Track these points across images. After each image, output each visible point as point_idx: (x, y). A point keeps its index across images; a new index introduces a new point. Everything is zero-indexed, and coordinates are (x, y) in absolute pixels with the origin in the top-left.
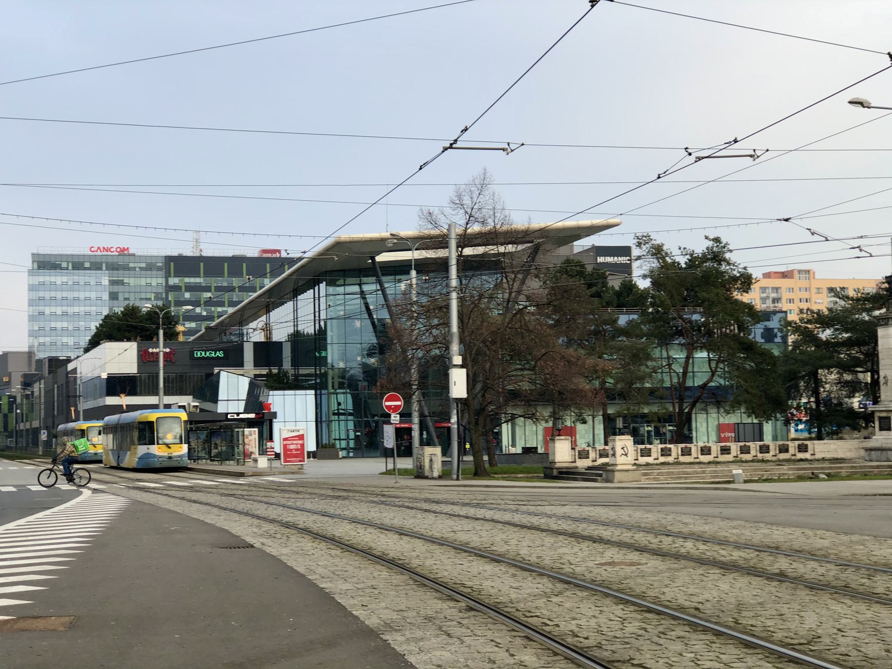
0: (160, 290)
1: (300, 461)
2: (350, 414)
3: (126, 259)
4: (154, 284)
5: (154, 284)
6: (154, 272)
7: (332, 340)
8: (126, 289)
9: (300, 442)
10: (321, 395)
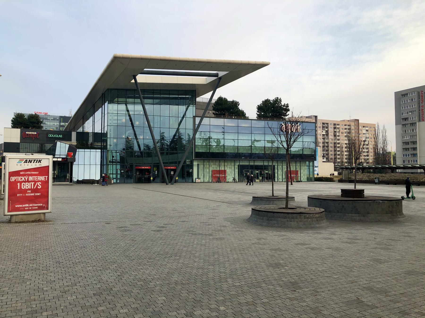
0: (58, 126)
1: (40, 208)
2: (118, 162)
3: (47, 116)
4: (56, 124)
5: (56, 124)
6: (56, 121)
7: (110, 136)
8: (46, 125)
9: (42, 178)
10: (103, 152)
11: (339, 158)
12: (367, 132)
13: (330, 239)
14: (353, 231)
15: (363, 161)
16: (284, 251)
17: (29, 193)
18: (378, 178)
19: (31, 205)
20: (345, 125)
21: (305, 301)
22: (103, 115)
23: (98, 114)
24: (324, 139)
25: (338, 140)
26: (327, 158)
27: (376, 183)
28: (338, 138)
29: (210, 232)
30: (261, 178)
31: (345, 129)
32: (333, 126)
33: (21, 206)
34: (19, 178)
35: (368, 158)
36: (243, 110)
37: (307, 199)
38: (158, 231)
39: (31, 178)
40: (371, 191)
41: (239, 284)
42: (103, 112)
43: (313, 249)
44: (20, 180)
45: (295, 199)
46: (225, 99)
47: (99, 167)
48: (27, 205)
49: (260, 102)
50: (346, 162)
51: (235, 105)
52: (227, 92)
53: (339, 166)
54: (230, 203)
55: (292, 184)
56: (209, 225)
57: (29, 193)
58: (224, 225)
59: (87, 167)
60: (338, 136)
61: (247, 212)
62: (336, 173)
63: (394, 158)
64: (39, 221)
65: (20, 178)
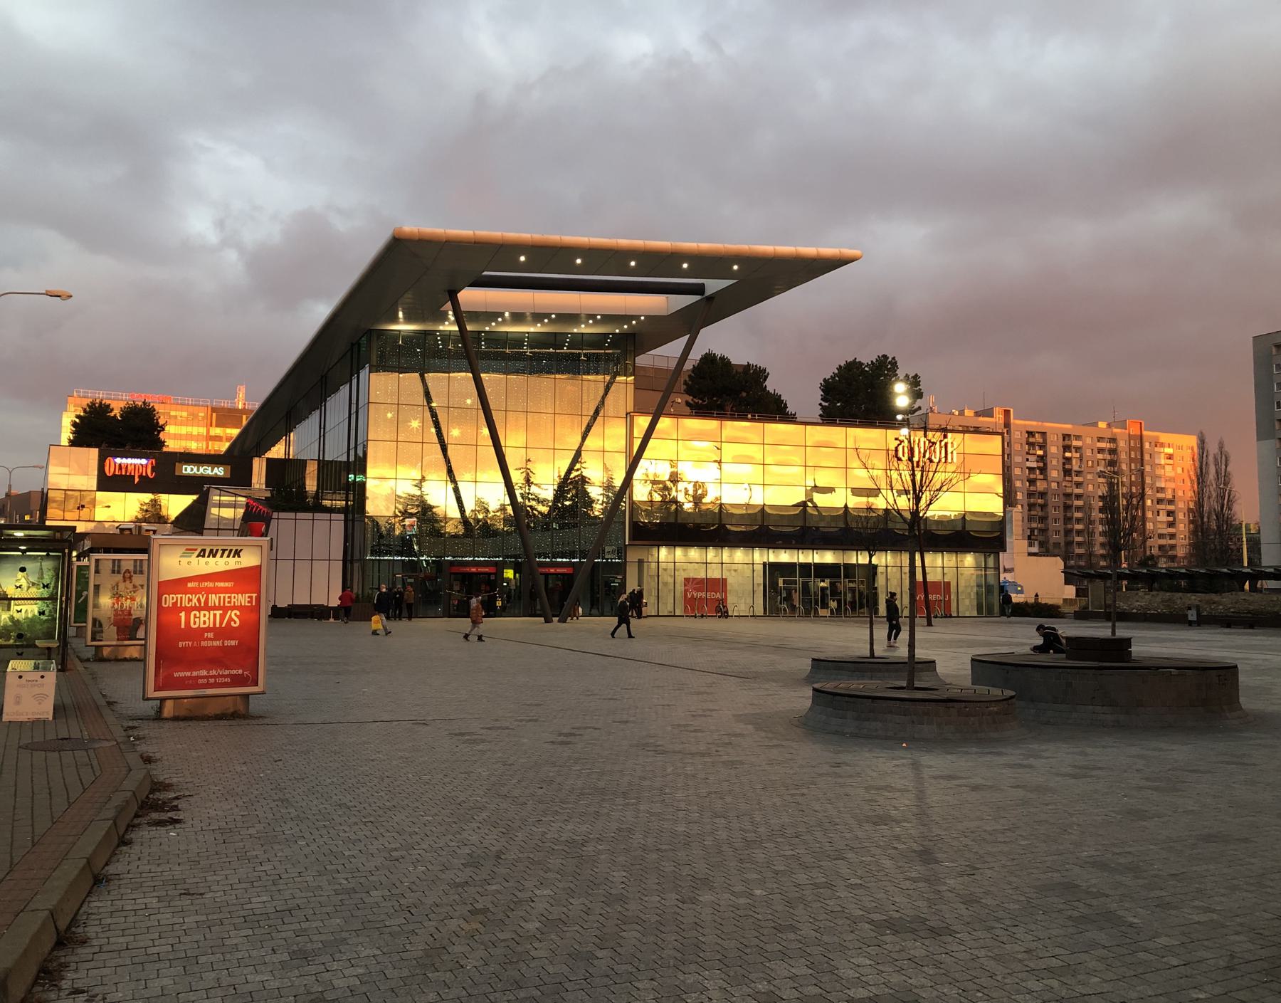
1: (237, 681)
10: (353, 521)
11: (1079, 544)
12: (1170, 462)
13: (1025, 766)
14: (1089, 750)
15: (1155, 551)
16: (899, 791)
17: (208, 639)
18: (1198, 607)
19: (214, 672)
20: (1100, 439)
21: (945, 884)
22: (354, 407)
23: (337, 404)
24: (1032, 482)
25: (1078, 485)
26: (1042, 544)
27: (1190, 623)
28: (1076, 479)
29: (702, 748)
30: (833, 605)
31: (1100, 451)
32: (1061, 442)
33: (188, 674)
34: (184, 599)
35: (1172, 542)
36: (778, 392)
37: (967, 669)
38: (562, 743)
39: (214, 599)
40: (1151, 644)
41: (791, 853)
42: (354, 401)
43: (975, 788)
44: (185, 603)
45: (940, 669)
46: (722, 358)
47: (339, 566)
48: (204, 673)
49: (829, 371)
50: (1102, 556)
51: (755, 376)
52: (727, 339)
53: (1080, 567)
54: (747, 677)
55: (930, 624)
56: (695, 731)
57: (208, 639)
58: (738, 731)
59: (303, 568)
60: (1078, 473)
61: (802, 699)
62: (1070, 591)
63: (1255, 545)
64: (235, 716)
65: (185, 598)
